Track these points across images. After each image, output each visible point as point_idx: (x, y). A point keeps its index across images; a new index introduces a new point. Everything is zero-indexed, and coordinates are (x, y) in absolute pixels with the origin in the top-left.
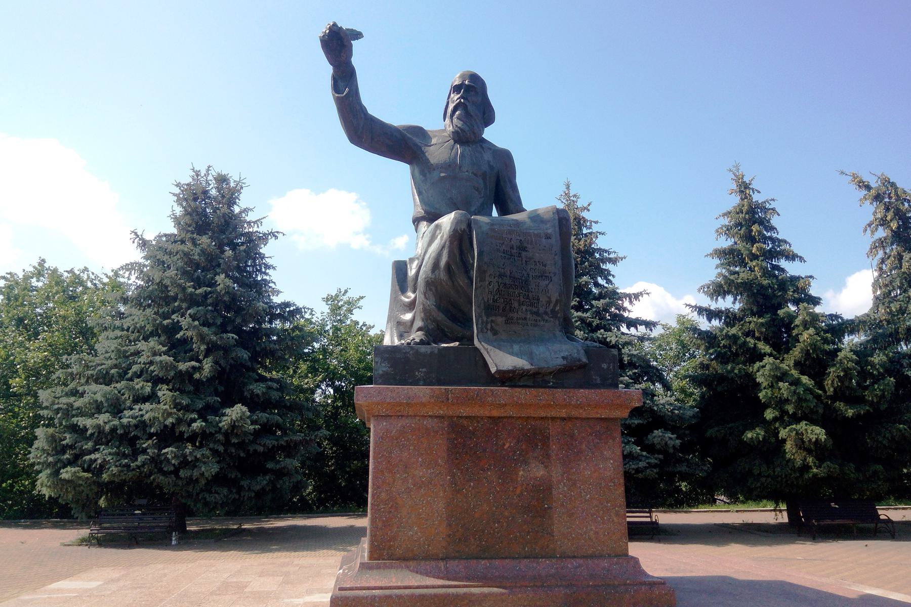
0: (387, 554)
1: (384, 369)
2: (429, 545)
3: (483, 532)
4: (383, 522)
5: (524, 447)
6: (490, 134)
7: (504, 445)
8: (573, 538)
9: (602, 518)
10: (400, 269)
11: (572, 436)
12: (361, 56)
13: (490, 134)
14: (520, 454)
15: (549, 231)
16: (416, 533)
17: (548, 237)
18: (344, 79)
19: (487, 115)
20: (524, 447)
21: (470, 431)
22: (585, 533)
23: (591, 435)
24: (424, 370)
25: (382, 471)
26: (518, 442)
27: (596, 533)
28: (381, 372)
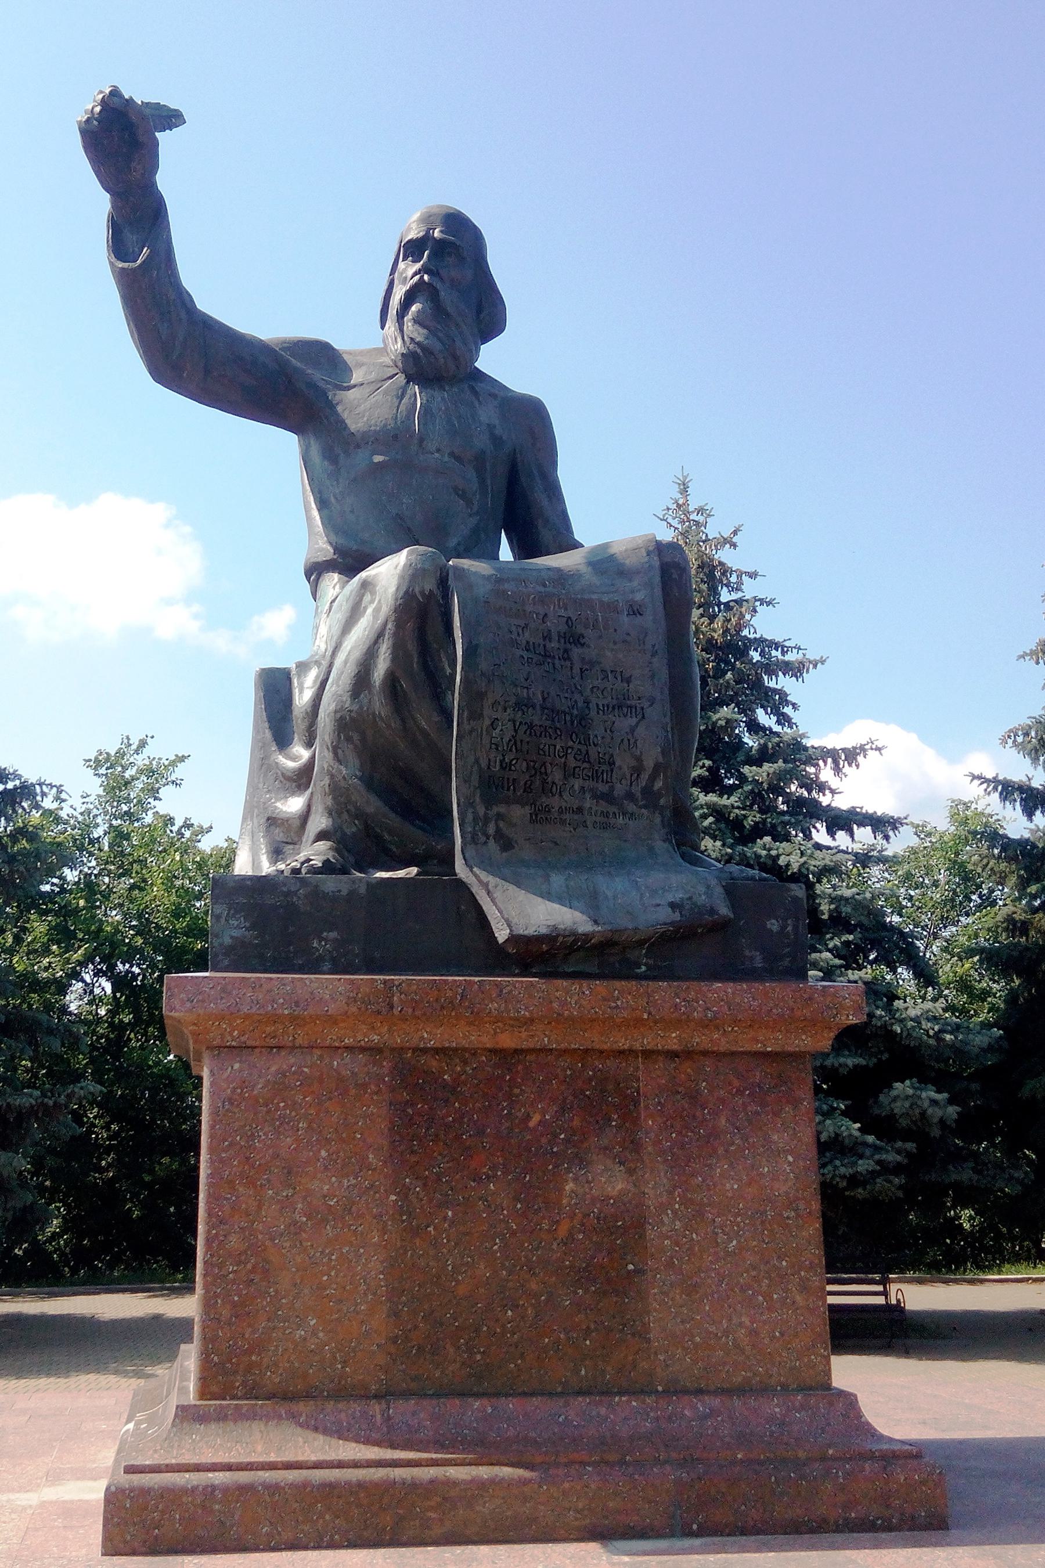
0: (244, 1383)
1: (236, 933)
2: (345, 1363)
3: (477, 1330)
4: (234, 1305)
5: (576, 1123)
6: (493, 359)
7: (528, 1117)
8: (696, 1346)
9: (768, 1297)
10: (275, 688)
11: (694, 1097)
12: (178, 169)
13: (493, 359)
14: (567, 1141)
15: (639, 597)
16: (314, 1334)
17: (635, 611)
18: (139, 224)
19: (487, 314)
20: (576, 1123)
21: (445, 1085)
22: (726, 1333)
23: (740, 1092)
24: (333, 935)
25: (231, 1183)
26: (563, 1109)
27: (754, 1333)
28: (227, 941)
